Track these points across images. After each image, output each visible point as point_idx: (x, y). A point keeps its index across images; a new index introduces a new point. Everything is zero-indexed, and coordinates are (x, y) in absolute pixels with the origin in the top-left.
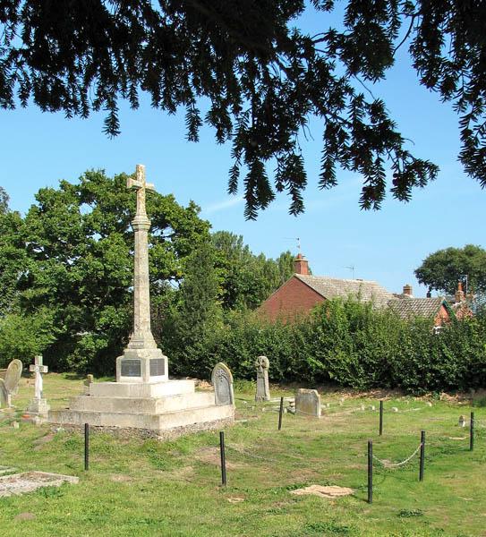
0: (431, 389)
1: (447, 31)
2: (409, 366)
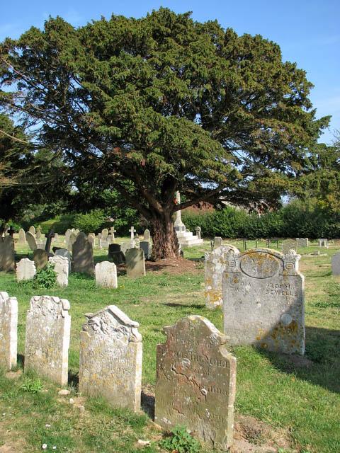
0: (258, 237)
1: (278, 106)
2: (250, 229)
